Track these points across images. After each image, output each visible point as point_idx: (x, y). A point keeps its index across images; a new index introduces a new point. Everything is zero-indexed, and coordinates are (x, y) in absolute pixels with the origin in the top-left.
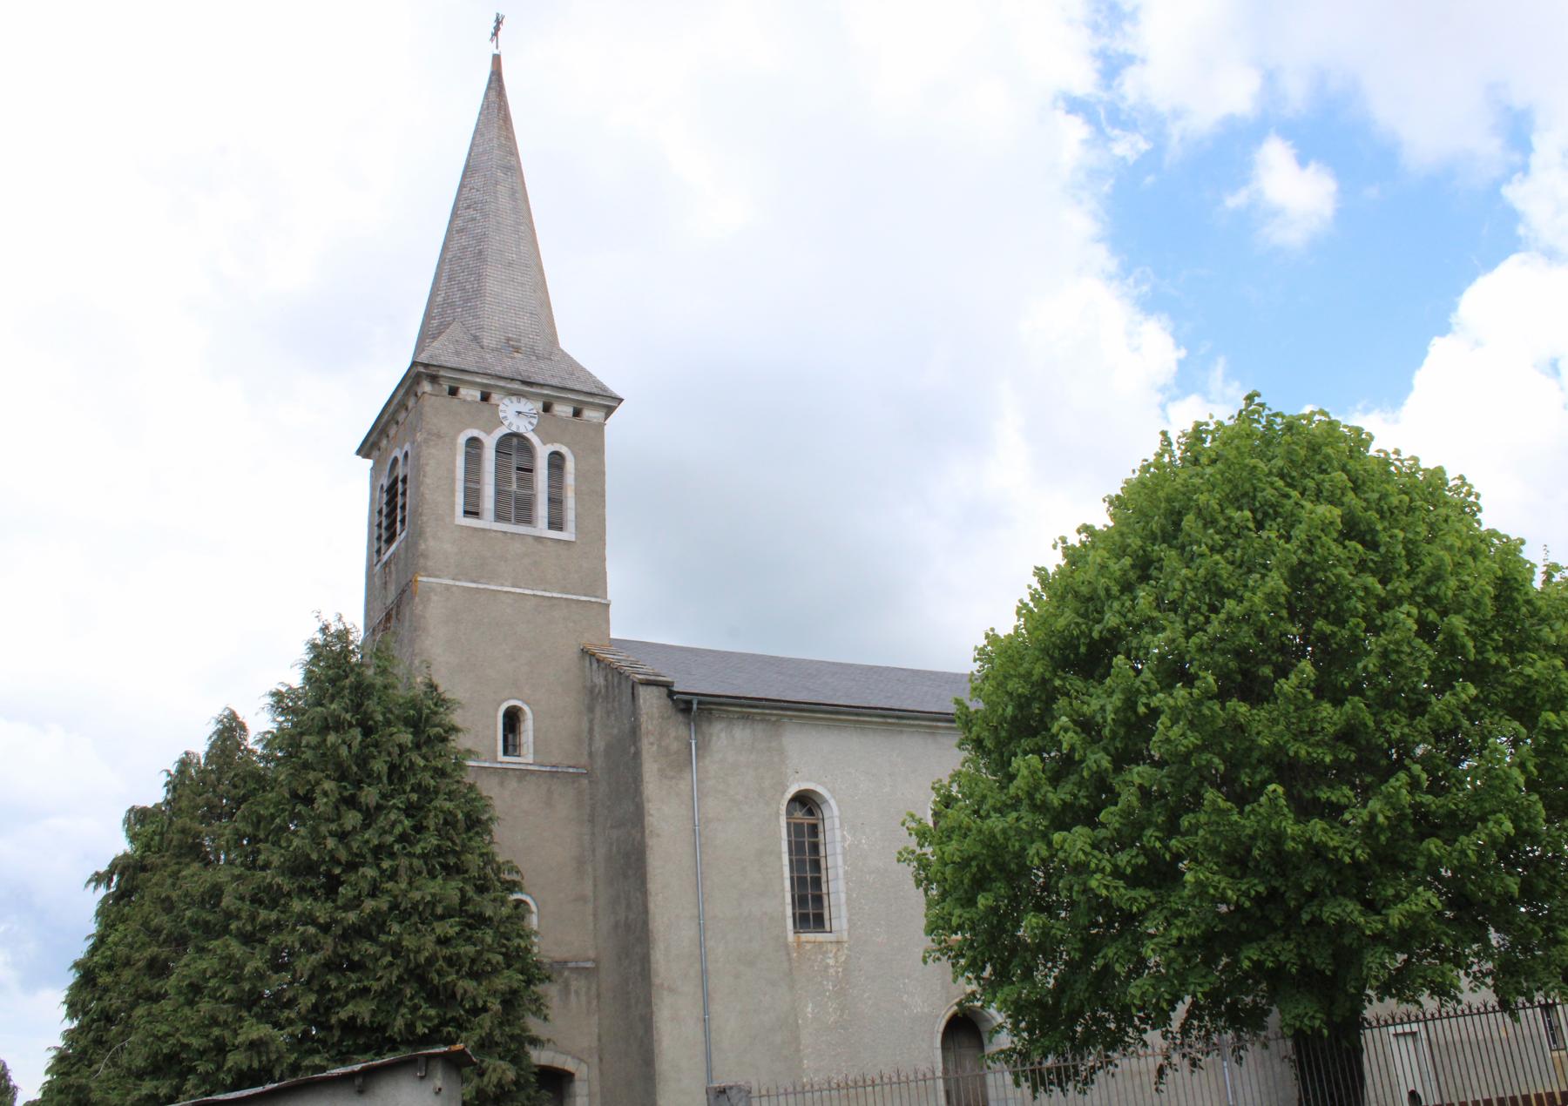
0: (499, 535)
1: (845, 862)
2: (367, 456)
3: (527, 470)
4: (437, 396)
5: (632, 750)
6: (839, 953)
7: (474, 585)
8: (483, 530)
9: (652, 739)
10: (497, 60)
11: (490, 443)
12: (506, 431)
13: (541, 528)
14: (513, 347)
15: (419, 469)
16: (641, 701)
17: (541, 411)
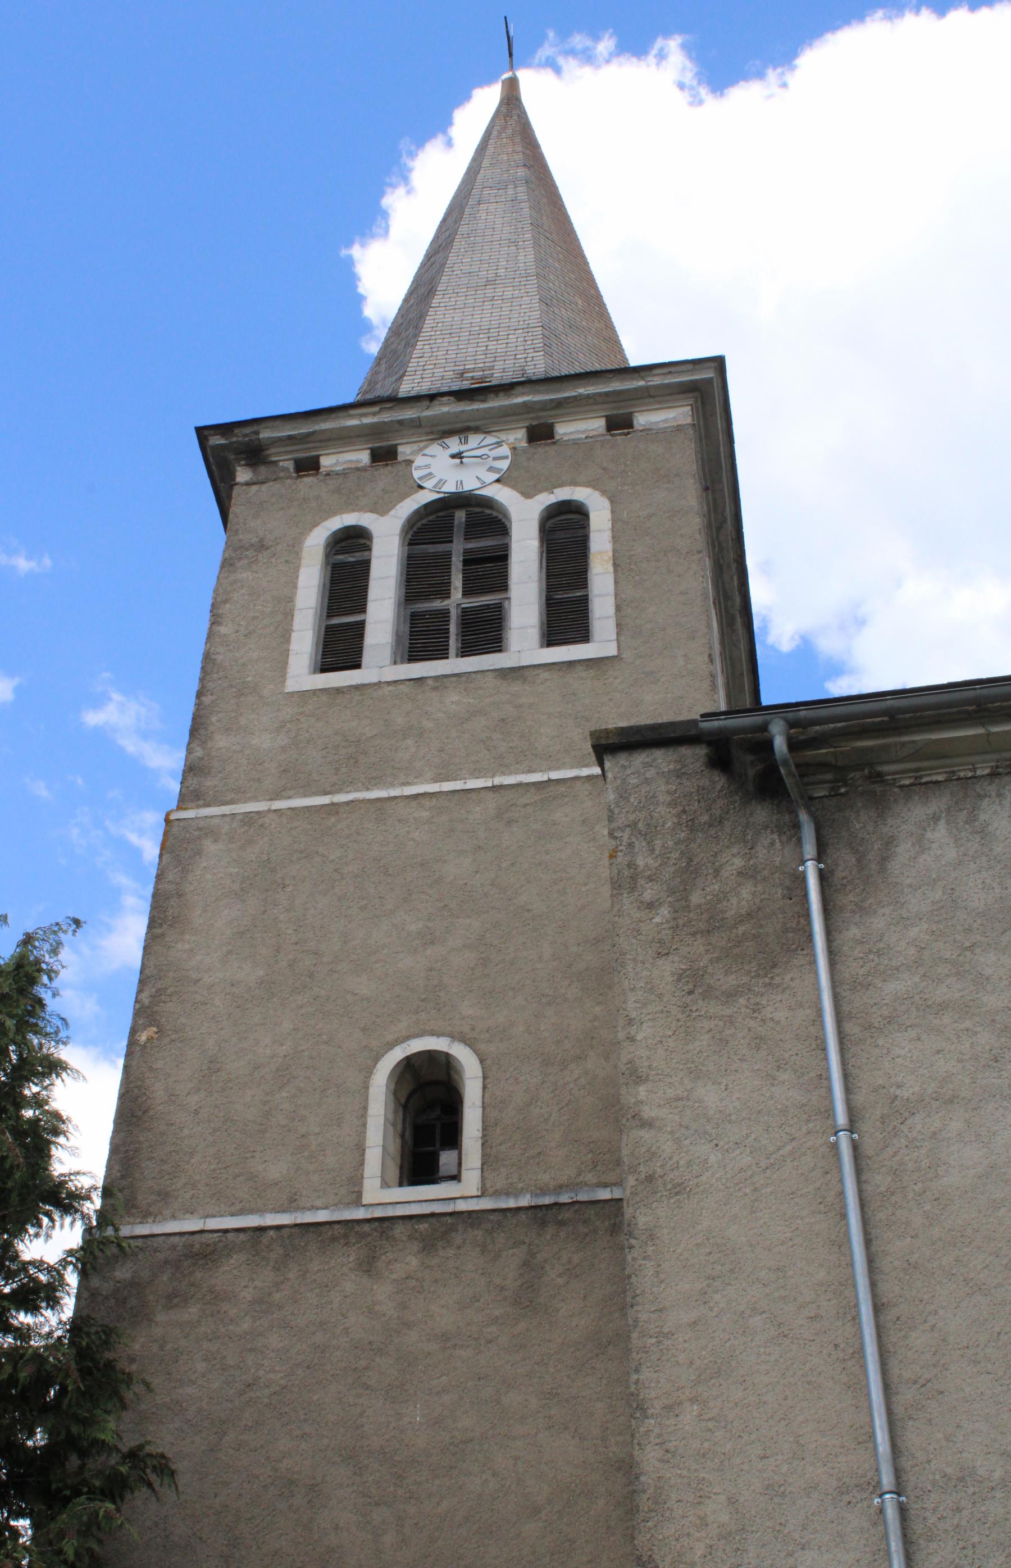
7: (325, 800)
17: (524, 444)
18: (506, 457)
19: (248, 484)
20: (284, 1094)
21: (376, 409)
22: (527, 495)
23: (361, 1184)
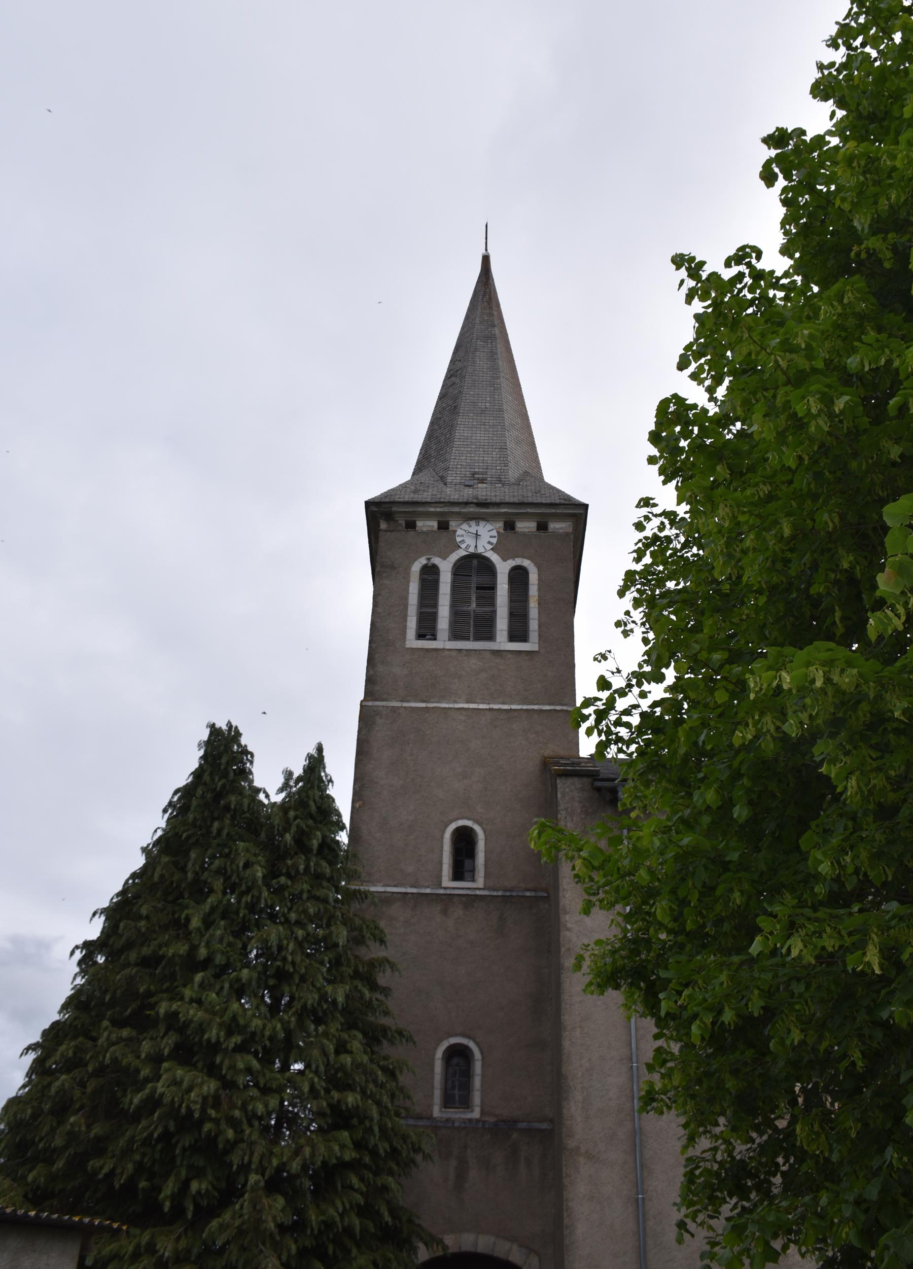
0: (454, 653)
4: (392, 531)
7: (423, 705)
8: (436, 650)
10: (486, 260)
11: (446, 567)
12: (462, 553)
13: (502, 642)
14: (478, 479)
16: (559, 795)
17: (502, 531)
18: (495, 537)
19: (386, 531)
20: (412, 837)
21: (442, 505)
22: (504, 559)
23: (441, 879)
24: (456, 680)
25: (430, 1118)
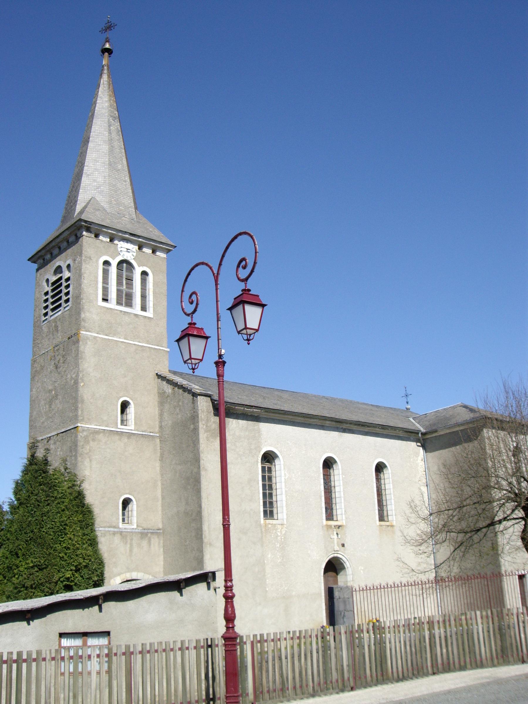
1: (286, 486)
2: (35, 262)
3: (130, 280)
5: (192, 427)
6: (283, 530)
9: (203, 422)
11: (114, 263)
15: (80, 276)
16: (199, 403)
17: (137, 249)
24: (120, 327)
25: (119, 528)
